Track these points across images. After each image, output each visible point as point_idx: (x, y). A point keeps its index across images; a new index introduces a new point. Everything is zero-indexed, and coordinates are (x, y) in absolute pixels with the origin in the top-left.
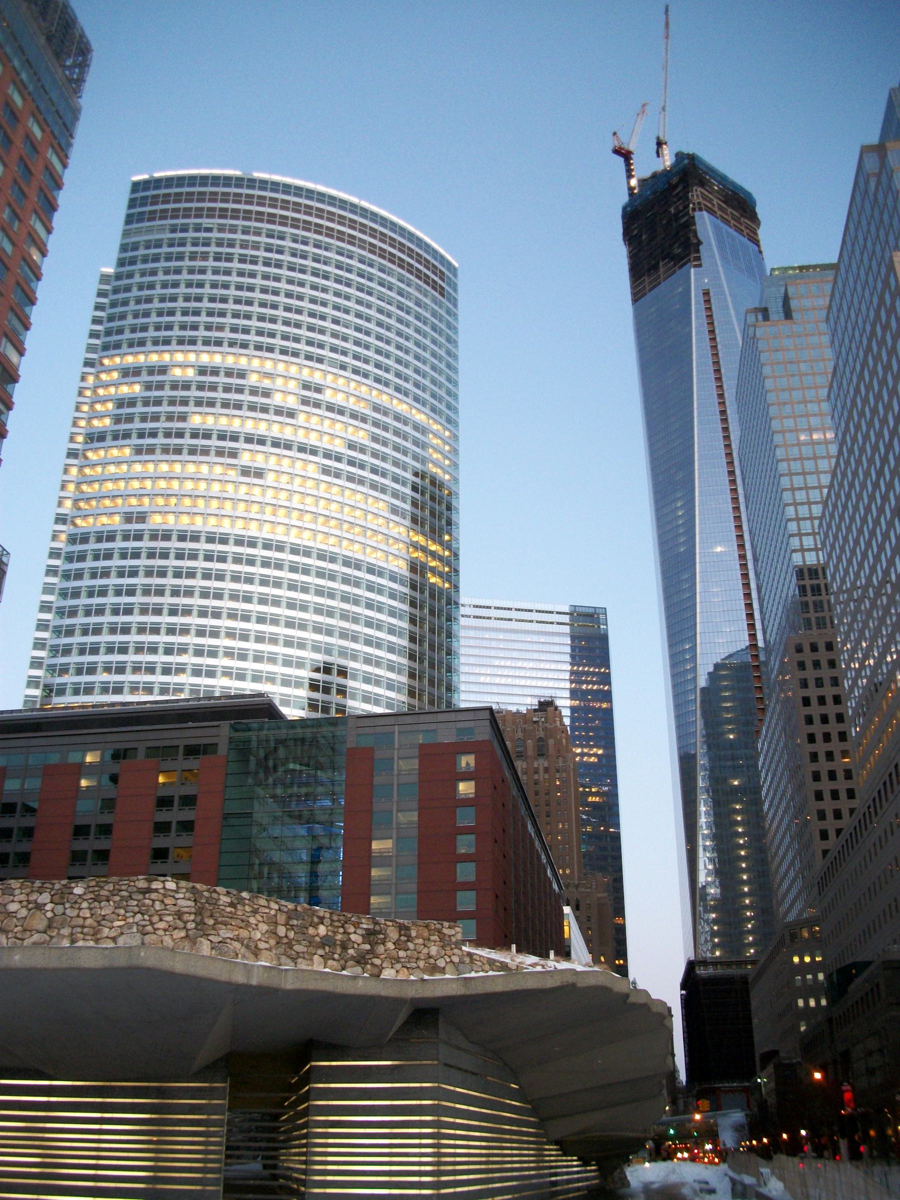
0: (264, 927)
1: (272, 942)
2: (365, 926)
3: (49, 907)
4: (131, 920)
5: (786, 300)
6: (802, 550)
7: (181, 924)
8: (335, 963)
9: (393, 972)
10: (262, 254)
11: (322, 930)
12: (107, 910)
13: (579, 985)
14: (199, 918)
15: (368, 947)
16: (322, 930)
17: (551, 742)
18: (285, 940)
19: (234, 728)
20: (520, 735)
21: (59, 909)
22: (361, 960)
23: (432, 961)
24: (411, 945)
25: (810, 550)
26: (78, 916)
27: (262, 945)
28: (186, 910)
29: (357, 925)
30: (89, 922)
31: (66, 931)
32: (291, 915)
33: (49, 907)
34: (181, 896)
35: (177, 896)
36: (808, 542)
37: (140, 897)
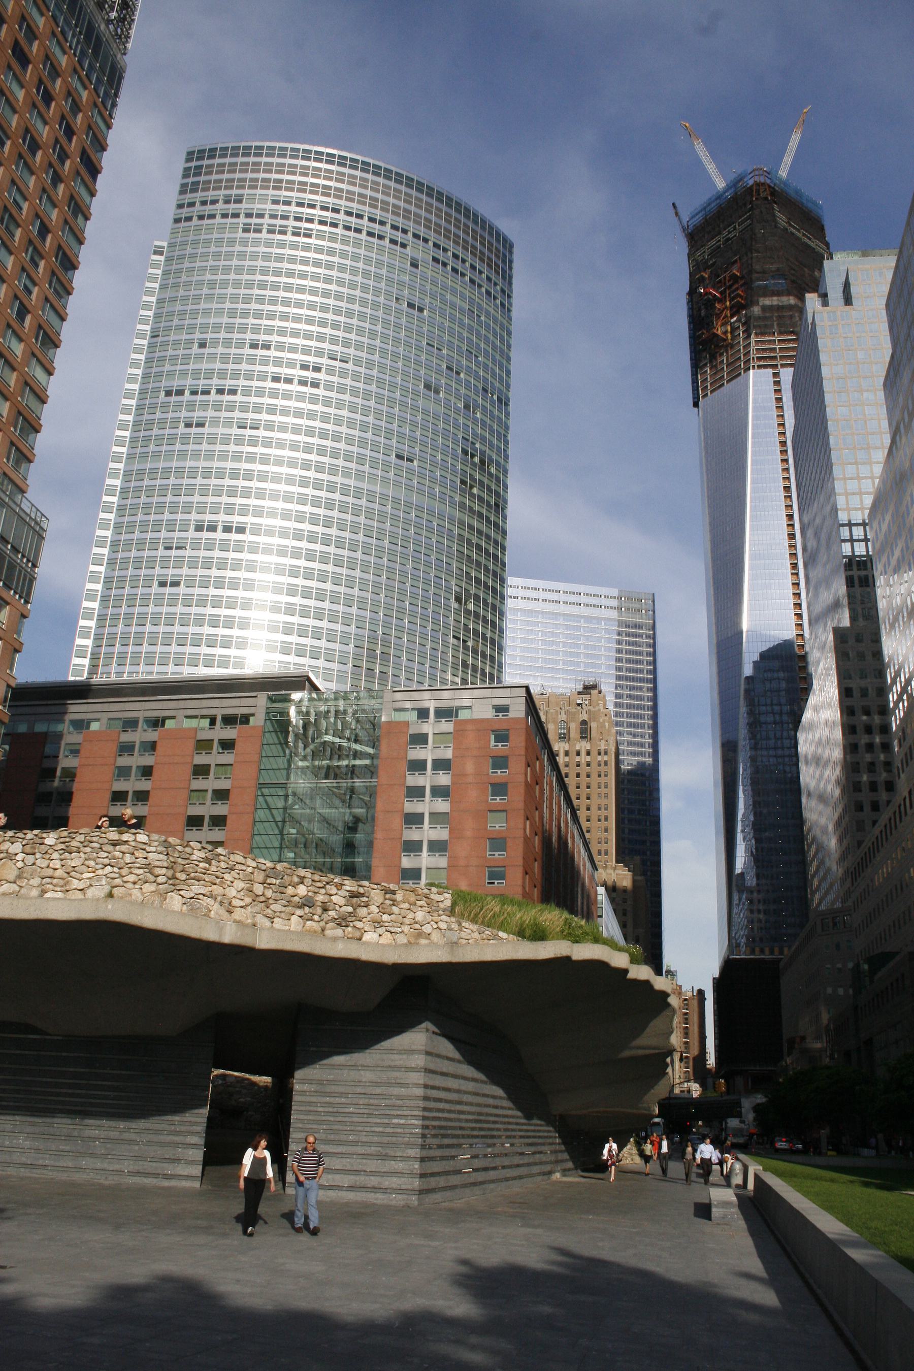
0: (240, 885)
1: (248, 900)
2: (348, 888)
3: (20, 856)
4: (100, 872)
5: (847, 286)
6: (852, 540)
7: (152, 878)
8: (314, 924)
9: (376, 936)
10: (294, 208)
11: (302, 890)
12: (75, 860)
13: (574, 958)
14: (170, 873)
15: (350, 909)
16: (302, 890)
17: (594, 725)
18: (262, 899)
19: (271, 700)
20: (564, 717)
21: (30, 859)
22: (342, 921)
23: (417, 926)
24: (395, 909)
25: (859, 540)
26: (48, 867)
27: (236, 903)
28: (157, 863)
29: (340, 886)
30: (59, 873)
31: (36, 881)
32: (270, 873)
33: (20, 856)
34: (154, 849)
35: (148, 849)
36: (858, 532)
37: (110, 848)
